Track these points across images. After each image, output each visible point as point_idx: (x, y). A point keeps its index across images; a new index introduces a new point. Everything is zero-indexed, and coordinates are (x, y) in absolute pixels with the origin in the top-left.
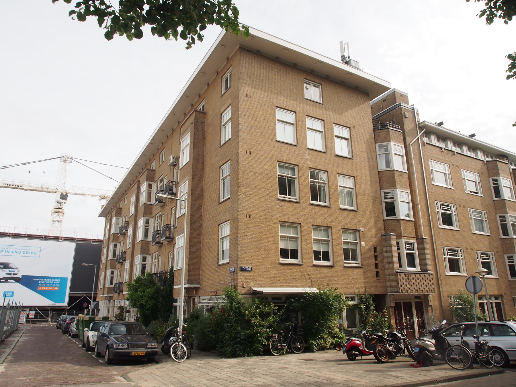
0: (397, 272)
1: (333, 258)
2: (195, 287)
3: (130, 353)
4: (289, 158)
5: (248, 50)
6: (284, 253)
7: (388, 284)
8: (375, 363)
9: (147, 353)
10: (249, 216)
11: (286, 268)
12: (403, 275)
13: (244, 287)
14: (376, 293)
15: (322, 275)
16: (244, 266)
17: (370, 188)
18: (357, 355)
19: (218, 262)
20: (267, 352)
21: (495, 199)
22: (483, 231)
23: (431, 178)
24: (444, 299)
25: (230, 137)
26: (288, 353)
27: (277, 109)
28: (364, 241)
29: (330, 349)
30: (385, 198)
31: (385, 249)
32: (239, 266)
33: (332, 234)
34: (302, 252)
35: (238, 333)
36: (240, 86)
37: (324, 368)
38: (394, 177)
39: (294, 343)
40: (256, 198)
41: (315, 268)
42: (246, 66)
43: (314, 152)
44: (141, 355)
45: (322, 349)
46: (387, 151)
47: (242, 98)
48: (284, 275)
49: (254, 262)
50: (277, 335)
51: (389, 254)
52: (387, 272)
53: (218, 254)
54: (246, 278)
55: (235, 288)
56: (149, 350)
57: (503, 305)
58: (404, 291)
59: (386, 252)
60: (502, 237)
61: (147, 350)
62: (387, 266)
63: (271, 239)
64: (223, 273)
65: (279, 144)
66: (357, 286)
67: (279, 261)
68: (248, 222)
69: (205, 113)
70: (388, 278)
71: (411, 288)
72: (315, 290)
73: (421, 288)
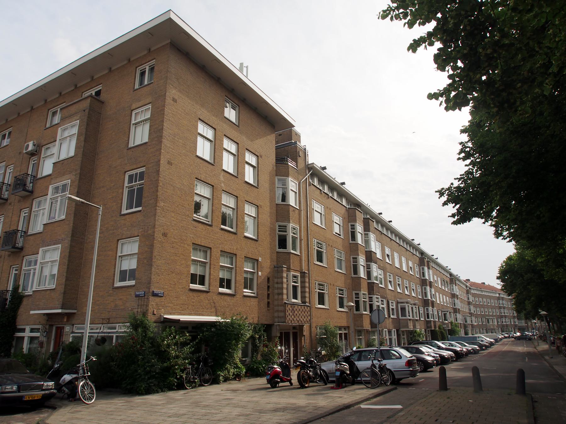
0: (285, 303)
1: (235, 287)
2: (66, 313)
3: (22, 397)
4: (206, 176)
5: (178, 49)
6: (194, 279)
7: (276, 314)
8: (298, 388)
9: (43, 395)
10: (165, 235)
11: (195, 294)
12: (289, 306)
13: (154, 314)
14: (266, 323)
15: (225, 303)
16: (156, 291)
17: (269, 220)
18: (278, 382)
19: (113, 284)
20: (180, 387)
21: (351, 242)
22: (341, 269)
23: (312, 217)
24: (313, 329)
25: (146, 139)
26: (201, 385)
27: (199, 122)
28: (261, 271)
29: (232, 379)
30: (279, 231)
31: (276, 280)
32: (151, 291)
33: (236, 262)
34: (210, 278)
35: (153, 366)
36: (167, 86)
37: (322, 390)
38: (289, 211)
39: (203, 375)
40: (173, 215)
41: (220, 296)
42: (175, 67)
43: (228, 175)
44: (36, 398)
45: (226, 380)
46: (285, 185)
47: (169, 101)
48: (193, 302)
49: (166, 287)
50: (190, 367)
51: (280, 286)
52: (276, 303)
53: (114, 274)
54: (157, 304)
55: (145, 314)
56: (47, 392)
57: (349, 335)
58: (289, 322)
59: (277, 283)
60: (353, 276)
61: (43, 392)
62: (276, 297)
63: (184, 262)
64: (121, 297)
65: (198, 159)
66: (252, 316)
67: (189, 286)
68: (164, 241)
69: (103, 103)
70: (276, 308)
71: (295, 319)
72: (219, 319)
73: (301, 319)
